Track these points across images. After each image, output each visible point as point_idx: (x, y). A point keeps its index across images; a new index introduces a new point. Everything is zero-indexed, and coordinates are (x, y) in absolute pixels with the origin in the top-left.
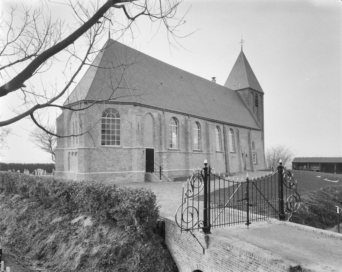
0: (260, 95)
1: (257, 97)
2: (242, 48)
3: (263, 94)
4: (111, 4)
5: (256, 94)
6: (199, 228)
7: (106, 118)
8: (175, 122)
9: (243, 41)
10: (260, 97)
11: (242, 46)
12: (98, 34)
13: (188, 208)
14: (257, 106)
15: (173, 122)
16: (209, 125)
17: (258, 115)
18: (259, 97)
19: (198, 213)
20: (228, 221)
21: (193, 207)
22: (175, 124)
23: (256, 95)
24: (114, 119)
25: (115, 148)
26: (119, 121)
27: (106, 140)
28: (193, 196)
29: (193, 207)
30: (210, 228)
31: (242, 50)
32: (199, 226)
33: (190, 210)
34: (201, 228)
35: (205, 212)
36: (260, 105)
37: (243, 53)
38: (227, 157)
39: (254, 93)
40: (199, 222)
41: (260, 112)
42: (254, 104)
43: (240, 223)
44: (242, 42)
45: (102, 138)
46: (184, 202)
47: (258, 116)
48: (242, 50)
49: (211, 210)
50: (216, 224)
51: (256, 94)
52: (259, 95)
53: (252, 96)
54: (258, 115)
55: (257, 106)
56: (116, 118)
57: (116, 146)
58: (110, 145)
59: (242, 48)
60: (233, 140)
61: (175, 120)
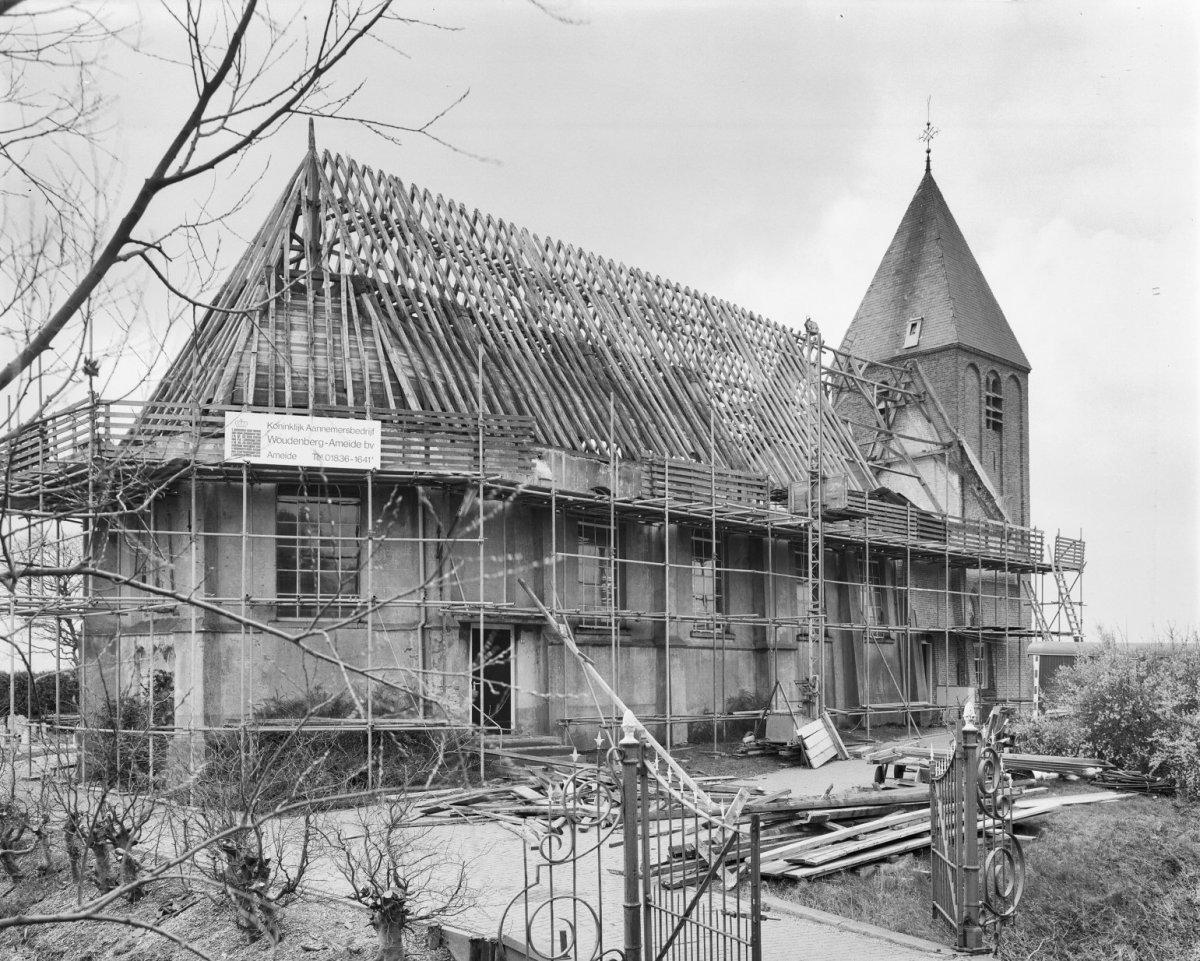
0: (1013, 377)
2: (928, 161)
3: (1026, 370)
4: (1068, 838)
5: (993, 372)
10: (1013, 383)
11: (928, 152)
12: (219, 118)
14: (997, 427)
16: (675, 743)
17: (1001, 468)
18: (1008, 390)
23: (992, 378)
24: (433, 503)
28: (571, 857)
31: (928, 169)
33: (564, 908)
35: (632, 914)
36: (1010, 423)
37: (931, 178)
38: (830, 674)
41: (1011, 456)
42: (984, 421)
45: (277, 585)
47: (1001, 476)
48: (928, 169)
51: (993, 372)
52: (1005, 376)
53: (971, 380)
54: (1001, 468)
55: (997, 427)
59: (928, 161)
60: (896, 612)
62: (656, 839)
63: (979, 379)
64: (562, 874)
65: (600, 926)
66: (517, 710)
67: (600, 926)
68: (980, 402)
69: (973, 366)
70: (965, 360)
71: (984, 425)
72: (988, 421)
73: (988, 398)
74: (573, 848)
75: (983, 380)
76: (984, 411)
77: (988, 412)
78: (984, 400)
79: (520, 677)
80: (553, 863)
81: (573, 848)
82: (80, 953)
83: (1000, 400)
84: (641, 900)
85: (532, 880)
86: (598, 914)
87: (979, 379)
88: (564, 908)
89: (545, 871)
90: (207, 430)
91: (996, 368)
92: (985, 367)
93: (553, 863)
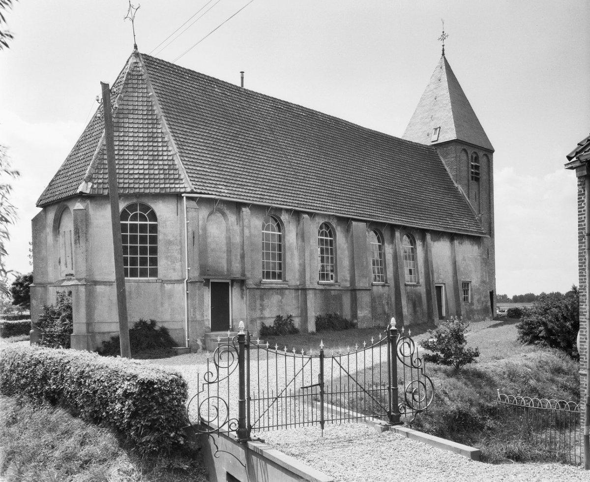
1: (476, 159)
2: (443, 50)
3: (494, 151)
5: (475, 153)
6: (230, 430)
7: (129, 222)
8: (275, 225)
9: (446, 35)
11: (443, 46)
13: (209, 399)
15: (272, 226)
19: (425, 387)
20: (284, 420)
21: (218, 398)
22: (276, 228)
23: (474, 156)
25: (148, 282)
26: (154, 228)
27: (139, 267)
28: (217, 381)
29: (218, 398)
30: (249, 432)
32: (229, 427)
33: (213, 401)
34: (233, 431)
35: (242, 404)
39: (469, 152)
40: (229, 420)
41: (484, 196)
43: (271, 429)
44: (444, 37)
46: (201, 389)
49: (252, 402)
50: (262, 425)
51: (475, 153)
52: (481, 154)
53: (464, 157)
56: (148, 223)
57: (149, 278)
58: (137, 277)
59: (443, 50)
61: (276, 221)
62: (313, 384)
63: (468, 156)
64: (213, 387)
65: (228, 409)
66: (232, 320)
67: (228, 409)
68: (468, 168)
69: (465, 150)
70: (460, 147)
71: (470, 179)
72: (472, 177)
73: (472, 165)
74: (218, 377)
75: (470, 157)
76: (470, 172)
77: (472, 172)
78: (470, 166)
79: (234, 304)
80: (209, 383)
81: (218, 377)
82: (4, 213)
83: (479, 166)
84: (246, 398)
85: (201, 389)
86: (227, 403)
87: (468, 156)
88: (213, 401)
89: (206, 386)
90: (156, 87)
91: (476, 150)
92: (470, 152)
93: (209, 383)
